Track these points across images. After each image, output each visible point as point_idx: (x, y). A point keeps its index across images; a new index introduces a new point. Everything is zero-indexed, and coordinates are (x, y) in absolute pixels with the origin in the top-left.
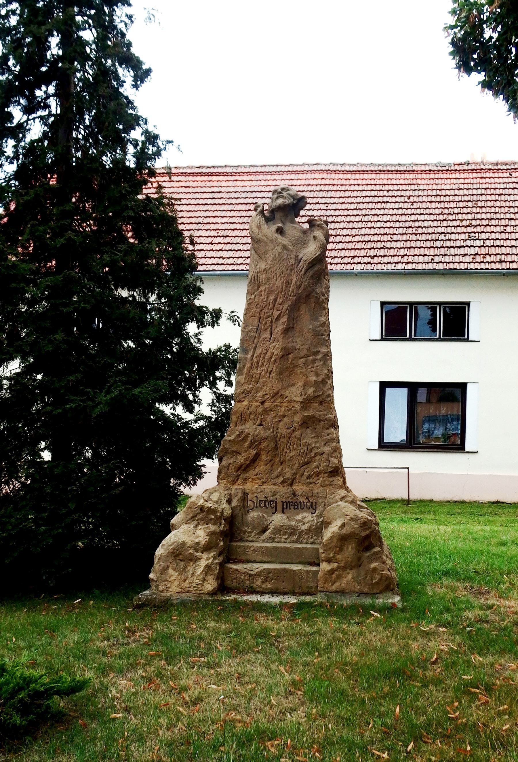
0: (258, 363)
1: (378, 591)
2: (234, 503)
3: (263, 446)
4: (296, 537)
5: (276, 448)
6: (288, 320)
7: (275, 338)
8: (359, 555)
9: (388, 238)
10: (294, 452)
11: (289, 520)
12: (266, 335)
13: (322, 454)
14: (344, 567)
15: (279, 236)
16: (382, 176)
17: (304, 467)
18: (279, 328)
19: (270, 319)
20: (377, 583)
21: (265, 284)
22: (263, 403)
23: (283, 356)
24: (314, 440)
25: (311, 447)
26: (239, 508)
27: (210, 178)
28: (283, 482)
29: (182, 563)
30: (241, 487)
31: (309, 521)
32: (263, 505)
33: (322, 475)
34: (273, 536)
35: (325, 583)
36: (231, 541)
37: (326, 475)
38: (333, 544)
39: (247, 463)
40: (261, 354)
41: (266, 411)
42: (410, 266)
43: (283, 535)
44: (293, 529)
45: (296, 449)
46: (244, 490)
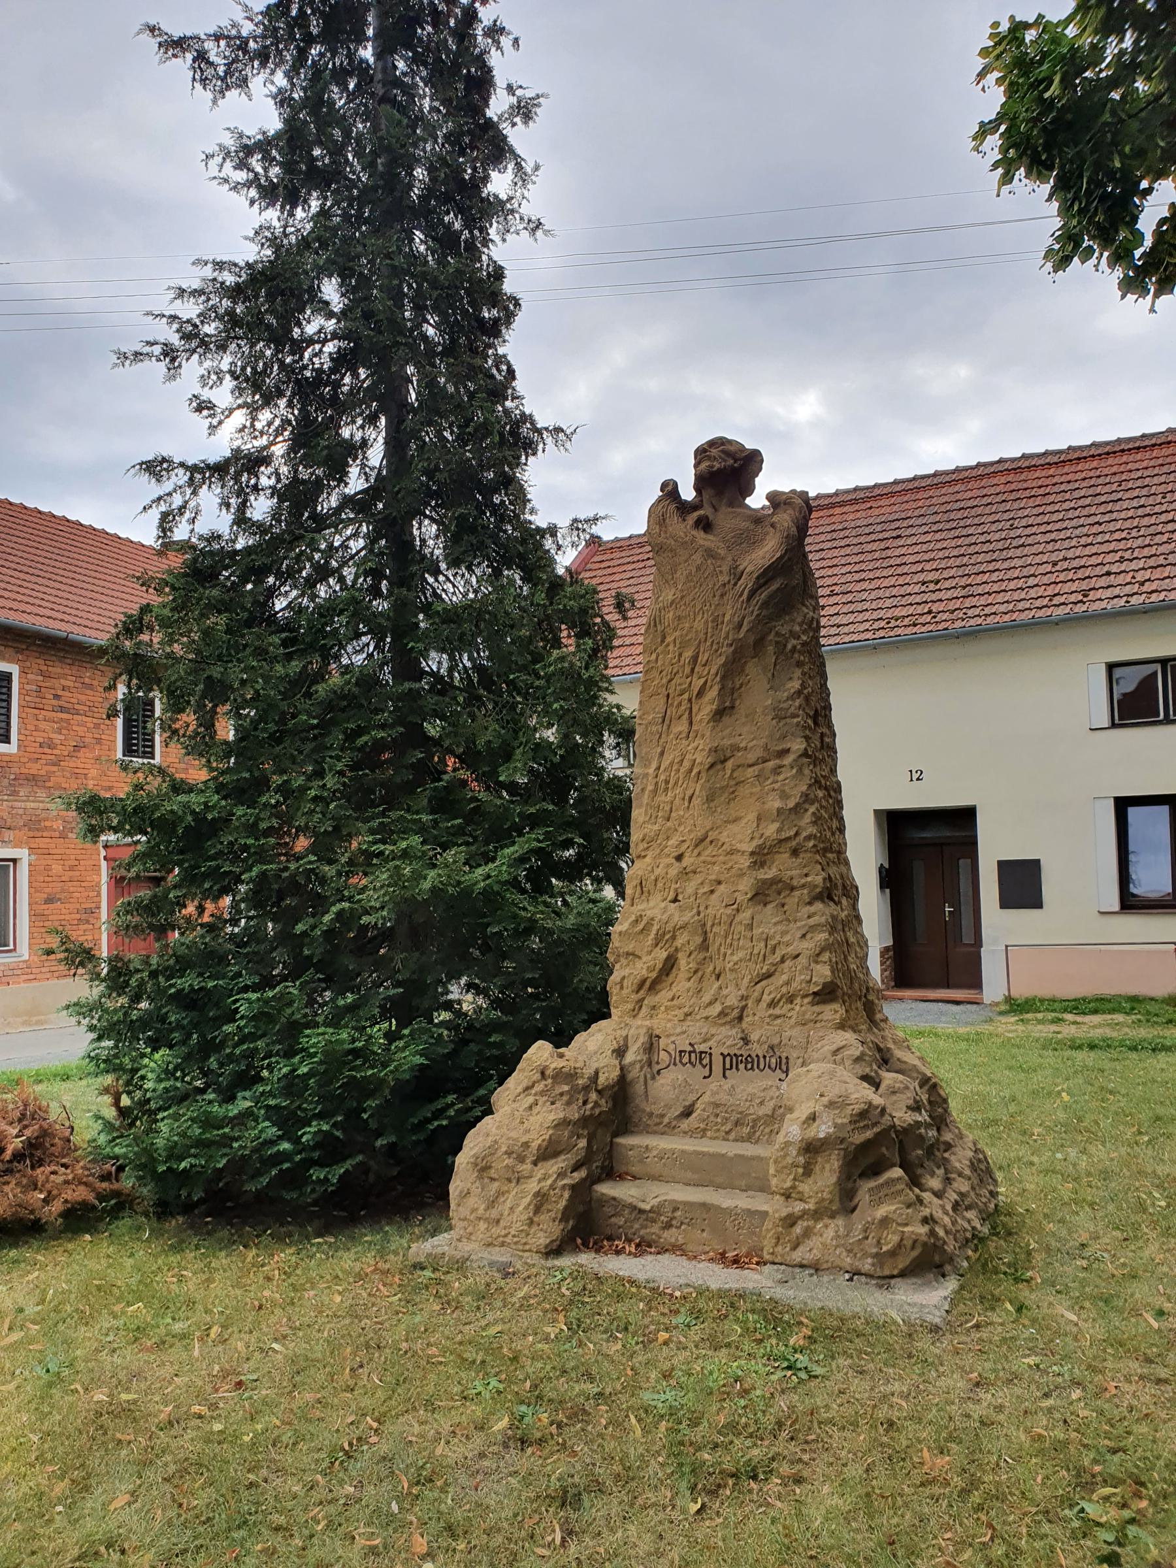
0: (667, 782)
1: (895, 1272)
2: (629, 1057)
3: (679, 942)
5: (704, 946)
6: (721, 693)
7: (697, 732)
8: (850, 1185)
10: (741, 954)
12: (681, 727)
14: (816, 1211)
15: (700, 535)
16: (1110, 461)
17: (763, 983)
19: (686, 696)
20: (893, 1253)
21: (675, 629)
22: (679, 858)
23: (712, 766)
25: (773, 942)
26: (638, 1066)
27: (831, 511)
28: (723, 1014)
30: (648, 1023)
33: (798, 1000)
35: (776, 1245)
36: (616, 1134)
37: (806, 1000)
38: (789, 1160)
39: (654, 975)
40: (672, 764)
41: (685, 873)
42: (1154, 598)
45: (743, 948)
46: (650, 1029)
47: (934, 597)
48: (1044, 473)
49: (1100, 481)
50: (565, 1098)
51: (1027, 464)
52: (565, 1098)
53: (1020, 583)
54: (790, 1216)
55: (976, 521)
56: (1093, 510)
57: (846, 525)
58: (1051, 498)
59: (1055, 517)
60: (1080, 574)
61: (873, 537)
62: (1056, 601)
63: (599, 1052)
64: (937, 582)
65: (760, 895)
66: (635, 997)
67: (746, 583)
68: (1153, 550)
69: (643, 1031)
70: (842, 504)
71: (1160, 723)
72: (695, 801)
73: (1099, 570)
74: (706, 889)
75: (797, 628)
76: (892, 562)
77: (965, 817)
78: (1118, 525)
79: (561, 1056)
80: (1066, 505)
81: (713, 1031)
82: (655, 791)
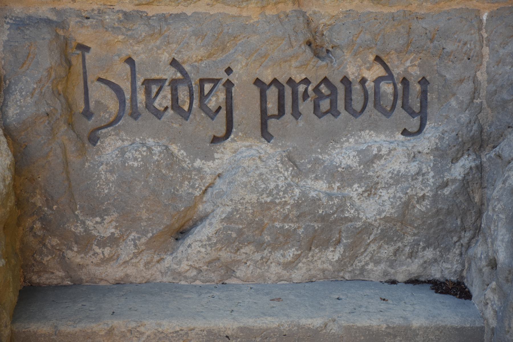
4: (334, 255)
11: (299, 172)
31: (397, 178)
32: (164, 99)
34: (225, 255)
43: (275, 246)
44: (323, 218)
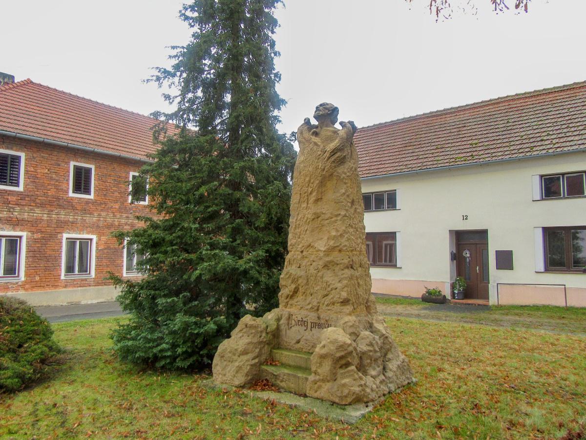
2: (281, 322)
3: (299, 282)
9: (422, 123)
13: (336, 289)
14: (323, 380)
16: (550, 96)
18: (312, 198)
22: (302, 252)
23: (313, 219)
24: (332, 278)
28: (312, 308)
29: (225, 363)
30: (289, 310)
39: (291, 293)
40: (301, 218)
41: (303, 257)
42: (558, 150)
46: (289, 312)
47: (474, 149)
48: (524, 101)
49: (545, 104)
50: (253, 335)
51: (517, 97)
52: (253, 335)
53: (507, 144)
54: (315, 380)
55: (495, 120)
56: (540, 115)
57: (446, 122)
58: (525, 111)
59: (525, 118)
60: (531, 140)
61: (455, 127)
62: (520, 151)
63: (271, 319)
64: (476, 144)
65: (326, 266)
66: (286, 301)
67: (327, 155)
68: (561, 131)
69: (287, 313)
70: (447, 114)
71: (561, 198)
72: (308, 232)
73: (539, 139)
74: (309, 263)
75: (346, 170)
76: (461, 136)
77: (483, 234)
78: (549, 121)
79: (255, 320)
80: (530, 114)
81: (309, 314)
82: (295, 228)
